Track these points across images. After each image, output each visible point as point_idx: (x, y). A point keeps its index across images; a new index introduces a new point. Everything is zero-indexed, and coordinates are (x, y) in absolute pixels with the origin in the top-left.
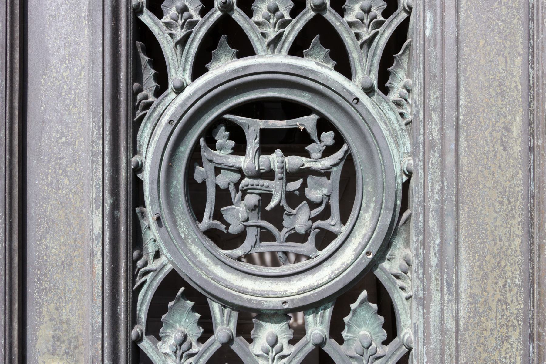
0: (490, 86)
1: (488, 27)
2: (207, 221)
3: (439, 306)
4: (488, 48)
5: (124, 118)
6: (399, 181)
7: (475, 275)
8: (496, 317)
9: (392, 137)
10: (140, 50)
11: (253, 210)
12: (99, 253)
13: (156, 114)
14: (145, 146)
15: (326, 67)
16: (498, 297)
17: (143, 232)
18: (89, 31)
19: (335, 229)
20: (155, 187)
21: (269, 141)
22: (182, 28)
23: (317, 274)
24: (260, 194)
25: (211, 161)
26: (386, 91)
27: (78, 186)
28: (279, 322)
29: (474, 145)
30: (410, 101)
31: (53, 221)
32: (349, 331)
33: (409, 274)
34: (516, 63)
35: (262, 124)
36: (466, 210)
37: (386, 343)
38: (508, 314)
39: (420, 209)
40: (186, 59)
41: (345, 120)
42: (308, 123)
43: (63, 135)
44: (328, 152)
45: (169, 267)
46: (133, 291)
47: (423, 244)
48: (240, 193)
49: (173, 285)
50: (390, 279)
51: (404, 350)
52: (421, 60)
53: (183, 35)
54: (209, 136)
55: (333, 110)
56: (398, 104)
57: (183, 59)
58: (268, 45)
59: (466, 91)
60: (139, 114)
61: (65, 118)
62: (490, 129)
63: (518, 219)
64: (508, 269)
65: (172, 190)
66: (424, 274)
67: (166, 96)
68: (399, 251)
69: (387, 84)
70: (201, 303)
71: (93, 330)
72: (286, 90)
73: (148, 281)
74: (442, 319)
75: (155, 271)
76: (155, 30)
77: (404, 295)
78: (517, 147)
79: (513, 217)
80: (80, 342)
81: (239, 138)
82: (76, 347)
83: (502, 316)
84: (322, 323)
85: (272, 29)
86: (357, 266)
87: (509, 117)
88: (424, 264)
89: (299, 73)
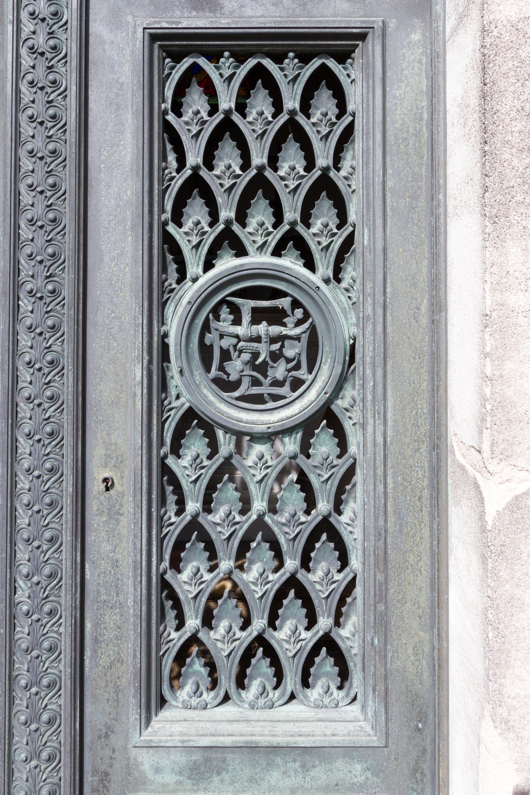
0: (407, 279)
1: (405, 239)
2: (214, 372)
3: (373, 428)
4: (405, 254)
5: (157, 300)
6: (348, 344)
7: (397, 407)
8: (411, 435)
9: (342, 313)
10: (166, 251)
11: (246, 364)
12: (140, 395)
13: (177, 297)
14: (170, 319)
15: (297, 264)
16: (412, 421)
17: (168, 381)
18: (132, 239)
19: (304, 377)
20: (179, 348)
21: (258, 316)
22: (197, 235)
23: (291, 408)
24: (251, 353)
25: (217, 330)
26: (338, 280)
27: (124, 348)
28: (264, 444)
29: (396, 319)
30: (355, 288)
31: (105, 372)
32: (313, 449)
33: (355, 408)
34: (424, 264)
35: (253, 303)
36: (391, 363)
37: (339, 457)
38: (419, 433)
39: (361, 362)
40: (200, 258)
41: (310, 301)
42: (284, 303)
43: (113, 312)
44: (299, 323)
45: (187, 405)
46: (162, 422)
47: (363, 386)
48: (237, 352)
49: (191, 417)
50: (341, 411)
51: (351, 461)
52: (361, 261)
53: (197, 241)
54: (216, 311)
55: (302, 294)
56: (347, 290)
57: (197, 258)
58: (257, 249)
59: (391, 282)
60: (166, 296)
61: (114, 300)
62: (407, 308)
63: (425, 369)
64: (419, 402)
65: (190, 350)
66: (363, 407)
67: (185, 284)
68: (349, 392)
69: (340, 276)
70: (209, 430)
71: (135, 448)
72: (270, 280)
73: (172, 415)
74: (375, 437)
75: (176, 408)
76: (177, 237)
77: (352, 422)
78: (425, 321)
79: (422, 367)
80: (125, 458)
81: (236, 311)
82: (122, 462)
83: (415, 434)
84: (295, 443)
85: (260, 237)
86: (318, 402)
87: (419, 300)
88: (363, 400)
89: (279, 269)
